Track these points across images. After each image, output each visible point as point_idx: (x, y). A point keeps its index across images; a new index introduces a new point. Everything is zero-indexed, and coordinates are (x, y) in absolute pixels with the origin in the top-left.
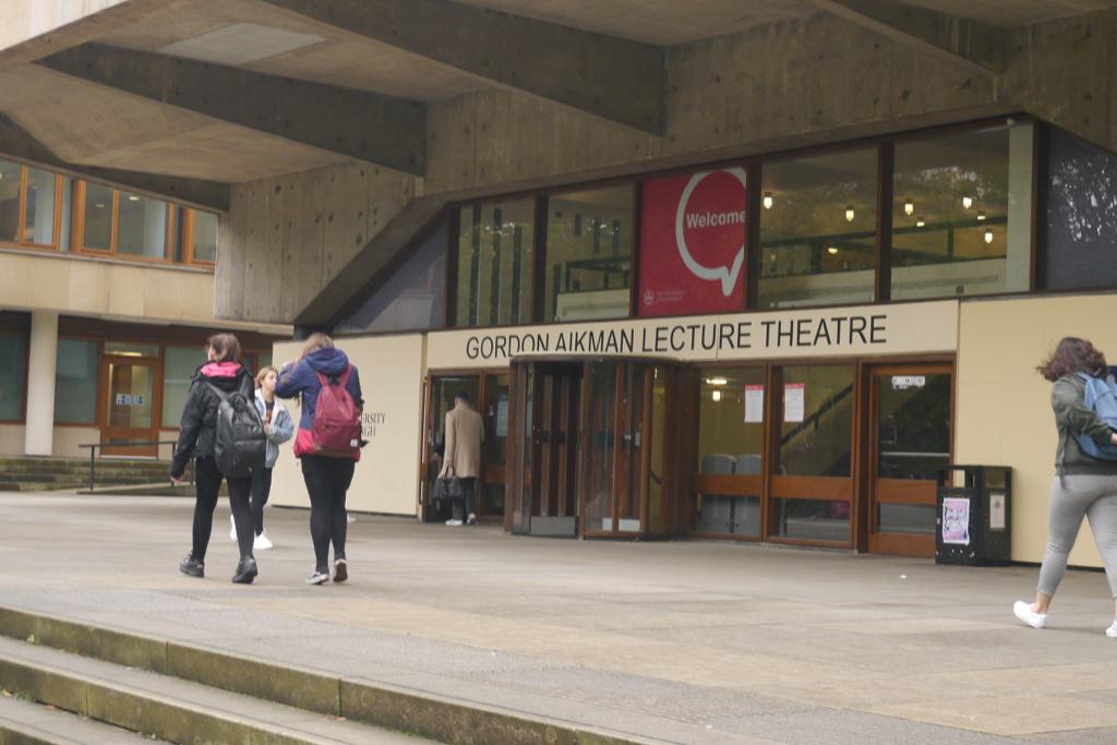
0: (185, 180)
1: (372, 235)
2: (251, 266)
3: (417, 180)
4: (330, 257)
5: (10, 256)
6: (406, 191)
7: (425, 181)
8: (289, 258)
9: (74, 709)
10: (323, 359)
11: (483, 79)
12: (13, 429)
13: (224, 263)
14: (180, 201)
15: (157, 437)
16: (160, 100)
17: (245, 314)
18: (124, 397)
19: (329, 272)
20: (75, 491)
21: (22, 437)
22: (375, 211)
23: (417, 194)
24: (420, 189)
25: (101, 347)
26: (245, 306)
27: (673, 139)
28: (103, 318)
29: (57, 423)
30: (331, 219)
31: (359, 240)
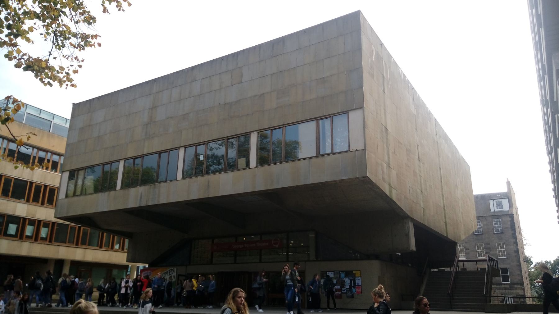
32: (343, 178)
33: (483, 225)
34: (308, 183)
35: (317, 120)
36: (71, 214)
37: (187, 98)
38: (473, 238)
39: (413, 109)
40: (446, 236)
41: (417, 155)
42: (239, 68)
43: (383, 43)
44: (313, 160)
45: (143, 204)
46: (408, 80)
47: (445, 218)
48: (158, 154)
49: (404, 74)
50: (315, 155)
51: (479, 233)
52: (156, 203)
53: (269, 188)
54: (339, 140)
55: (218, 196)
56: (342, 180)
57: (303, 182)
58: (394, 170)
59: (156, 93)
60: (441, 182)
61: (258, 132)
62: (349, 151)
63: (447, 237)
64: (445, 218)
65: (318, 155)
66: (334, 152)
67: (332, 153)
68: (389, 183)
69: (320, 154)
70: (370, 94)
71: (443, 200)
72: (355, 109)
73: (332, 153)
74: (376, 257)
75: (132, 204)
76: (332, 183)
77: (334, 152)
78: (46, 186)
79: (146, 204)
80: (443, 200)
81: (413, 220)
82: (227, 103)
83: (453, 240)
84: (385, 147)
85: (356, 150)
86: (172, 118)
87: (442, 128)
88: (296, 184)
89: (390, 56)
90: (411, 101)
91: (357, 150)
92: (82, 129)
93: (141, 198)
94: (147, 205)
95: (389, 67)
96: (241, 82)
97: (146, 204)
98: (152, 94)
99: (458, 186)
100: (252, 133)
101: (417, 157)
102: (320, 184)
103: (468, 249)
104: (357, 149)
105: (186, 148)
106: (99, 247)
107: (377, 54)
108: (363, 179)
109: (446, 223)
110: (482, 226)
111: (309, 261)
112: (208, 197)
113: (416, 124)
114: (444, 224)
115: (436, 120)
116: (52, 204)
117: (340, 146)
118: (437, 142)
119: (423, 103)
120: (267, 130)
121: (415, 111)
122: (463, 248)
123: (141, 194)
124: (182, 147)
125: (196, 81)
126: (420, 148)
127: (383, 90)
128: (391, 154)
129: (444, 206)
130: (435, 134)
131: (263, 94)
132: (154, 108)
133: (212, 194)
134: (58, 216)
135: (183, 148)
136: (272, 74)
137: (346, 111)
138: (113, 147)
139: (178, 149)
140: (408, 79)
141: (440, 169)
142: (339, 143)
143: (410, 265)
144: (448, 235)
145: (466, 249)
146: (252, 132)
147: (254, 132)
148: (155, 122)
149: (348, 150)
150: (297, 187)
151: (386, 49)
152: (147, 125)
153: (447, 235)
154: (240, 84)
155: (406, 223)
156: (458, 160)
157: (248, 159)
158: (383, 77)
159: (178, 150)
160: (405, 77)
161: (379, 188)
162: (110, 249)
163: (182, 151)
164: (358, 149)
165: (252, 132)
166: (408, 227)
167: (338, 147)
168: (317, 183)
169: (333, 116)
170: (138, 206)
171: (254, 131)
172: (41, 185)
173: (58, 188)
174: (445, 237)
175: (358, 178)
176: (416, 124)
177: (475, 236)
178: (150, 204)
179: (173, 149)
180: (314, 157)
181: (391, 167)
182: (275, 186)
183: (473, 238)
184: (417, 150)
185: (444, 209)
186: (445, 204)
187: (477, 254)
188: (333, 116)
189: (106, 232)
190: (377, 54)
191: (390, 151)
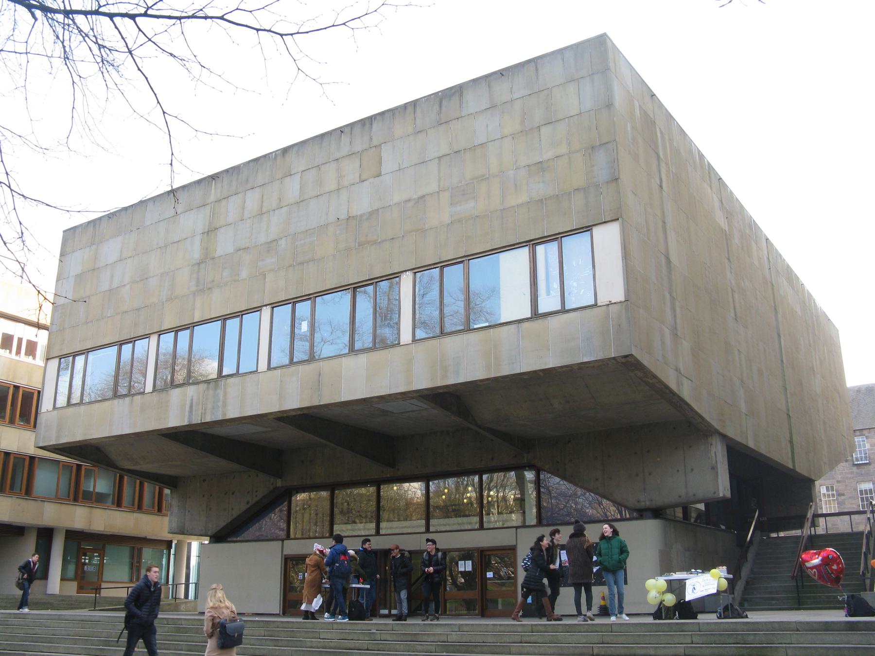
0: (162, 475)
1: (254, 501)
2: (189, 511)
3: (278, 480)
4: (232, 509)
5: (54, 503)
6: (272, 484)
7: (282, 481)
8: (210, 509)
9: (714, 611)
10: (395, 567)
11: (316, 438)
12: (42, 582)
13: (175, 510)
14: (141, 478)
15: (100, 585)
16: (198, 449)
17: (186, 532)
18: (87, 567)
19: (232, 515)
20: (87, 610)
21: (46, 586)
22: (256, 492)
23: (278, 486)
24: (279, 483)
25: (79, 545)
26: (186, 528)
27: (398, 470)
28: (14, 524)
29: (61, 580)
30: (233, 493)
31: (248, 503)
32: (586, 360)
33: (871, 445)
34: (517, 370)
35: (531, 245)
36: (64, 440)
37: (274, 210)
38: (852, 473)
39: (720, 219)
40: (791, 467)
41: (732, 311)
42: (375, 146)
43: (655, 93)
44: (526, 325)
45: (196, 420)
46: (709, 164)
47: (791, 433)
48: (117, 346)
49: (699, 151)
50: (529, 315)
51: (863, 462)
52: (220, 418)
53: (439, 383)
54: (575, 284)
55: (339, 401)
56: (582, 363)
57: (506, 370)
58: (685, 340)
59: (216, 201)
60: (782, 361)
61: (415, 273)
62: (595, 305)
63: (794, 471)
64: (791, 433)
65: (536, 315)
66: (566, 308)
67: (564, 311)
68: (676, 367)
69: (539, 313)
70: (633, 192)
71: (786, 398)
72: (605, 222)
73: (564, 311)
74: (657, 513)
75: (175, 420)
76: (564, 369)
77: (566, 308)
78: (17, 388)
79: (201, 420)
80: (786, 398)
81: (724, 437)
82: (353, 217)
83: (806, 474)
84: (668, 295)
85: (608, 303)
86: (246, 249)
87: (780, 254)
88: (493, 374)
89: (670, 118)
90: (717, 203)
91: (611, 303)
92: (80, 278)
93: (191, 407)
94: (203, 421)
95: (670, 139)
96: (379, 175)
97: (201, 420)
98: (208, 204)
99: (815, 370)
100: (402, 275)
101: (733, 315)
102: (541, 374)
103: (843, 495)
104: (610, 302)
105: (275, 308)
106: (116, 505)
107: (644, 114)
108: (624, 360)
109: (791, 442)
110: (869, 447)
111: (524, 526)
112: (320, 405)
113: (728, 250)
114: (789, 445)
115: (767, 239)
116: (28, 421)
117: (579, 296)
118: (772, 285)
119: (742, 207)
120: (433, 267)
121: (725, 224)
122: (833, 493)
123: (192, 400)
124: (266, 305)
125: (291, 175)
126: (736, 296)
127: (659, 184)
128: (678, 310)
129: (788, 410)
130: (767, 267)
131: (424, 196)
132: (211, 231)
133: (327, 397)
134: (41, 445)
135: (268, 307)
136: (439, 158)
137: (587, 227)
138: (138, 309)
139: (258, 311)
140: (707, 161)
141: (779, 336)
142: (576, 291)
143: (723, 527)
144: (796, 467)
145: (839, 495)
146: (402, 272)
147: (407, 273)
148: (213, 258)
149: (594, 303)
150: (496, 379)
151: (661, 105)
152: (199, 264)
153: (794, 466)
154: (376, 178)
155: (711, 445)
156: (814, 317)
157: (83, 605)
158: (659, 158)
159: (148, 339)
160: (701, 156)
161: (655, 377)
162: (136, 509)
163: (406, 280)
164: (613, 302)
165: (402, 272)
166: (715, 452)
167: (573, 299)
168: (535, 372)
169: (561, 237)
170: (186, 423)
171: (406, 271)
172: (8, 385)
173: (39, 392)
174: (792, 469)
175: (614, 358)
176: (728, 250)
177: (855, 469)
178: (208, 419)
179: (249, 311)
180: (527, 319)
181: (679, 334)
182: (452, 380)
183: (852, 473)
184: (731, 300)
185: (788, 415)
186: (789, 405)
187: (860, 503)
188: (561, 237)
189: (127, 476)
190: (644, 114)
191: (677, 304)
